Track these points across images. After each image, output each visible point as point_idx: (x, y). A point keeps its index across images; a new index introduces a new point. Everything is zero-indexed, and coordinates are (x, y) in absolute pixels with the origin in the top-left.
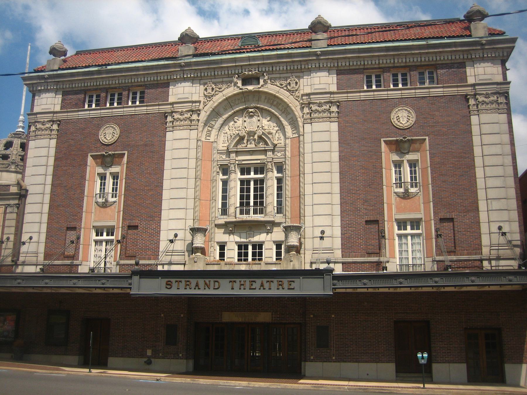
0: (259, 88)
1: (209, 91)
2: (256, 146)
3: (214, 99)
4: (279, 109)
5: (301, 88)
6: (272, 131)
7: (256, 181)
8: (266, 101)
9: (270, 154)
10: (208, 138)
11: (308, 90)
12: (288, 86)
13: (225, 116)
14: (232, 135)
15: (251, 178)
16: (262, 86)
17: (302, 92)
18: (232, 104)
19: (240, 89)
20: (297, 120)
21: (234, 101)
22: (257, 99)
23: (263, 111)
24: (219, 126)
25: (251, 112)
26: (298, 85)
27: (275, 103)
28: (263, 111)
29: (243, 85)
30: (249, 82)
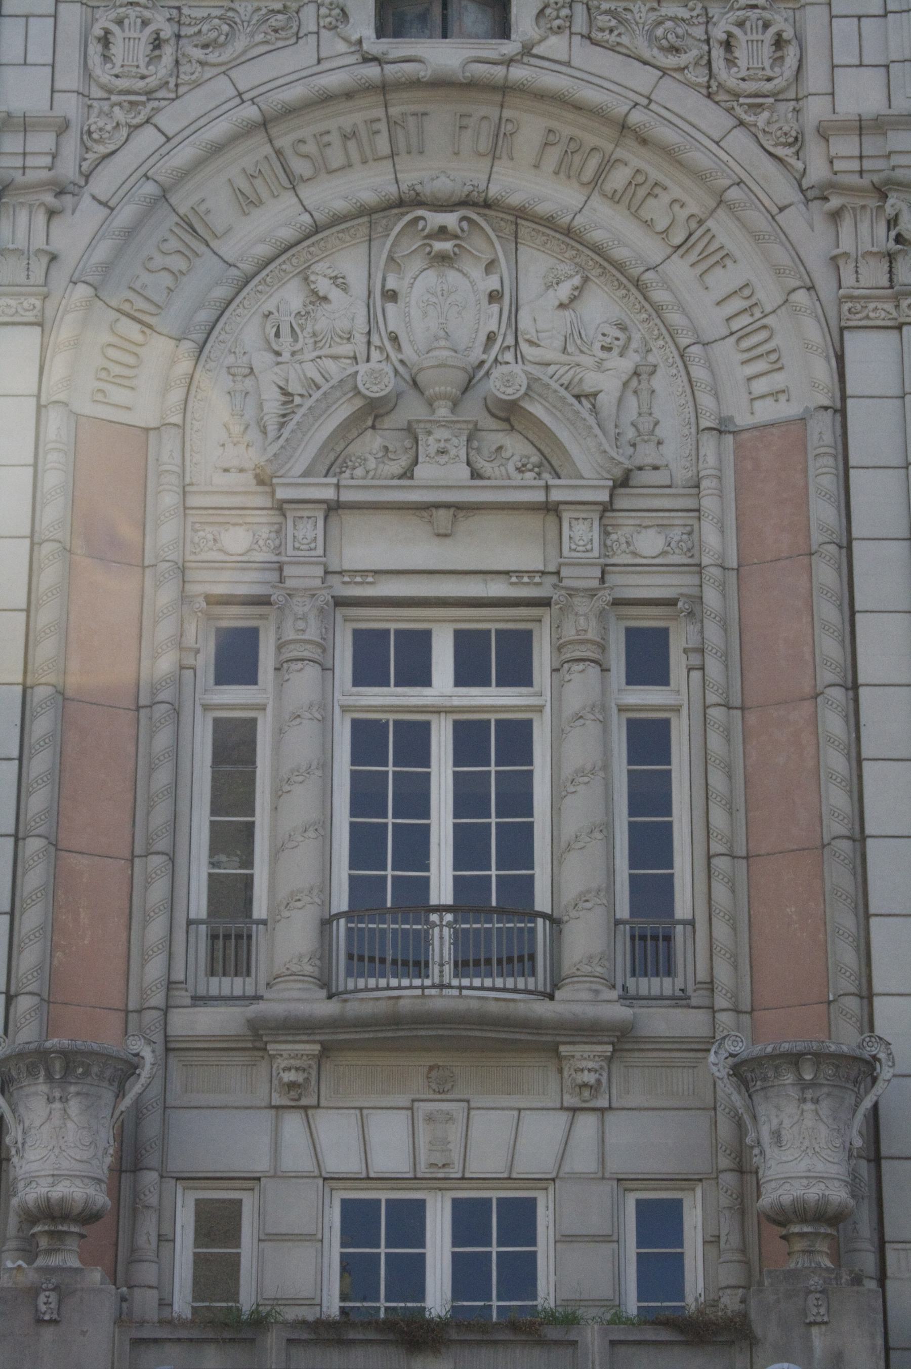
0: (509, 62)
1: (130, 48)
2: (476, 474)
3: (171, 119)
4: (648, 224)
5: (815, 78)
6: (592, 381)
7: (470, 737)
8: (553, 156)
9: (581, 533)
10: (119, 395)
11: (861, 95)
12: (719, 63)
13: (330, 195)
14: (294, 387)
15: (438, 711)
16: (527, 50)
17: (816, 110)
18: (300, 167)
19: (367, 59)
20: (8, 1160)
21: (310, 148)
22: (484, 145)
23: (525, 228)
24: (340, 206)
25: (442, 232)
26: (791, 61)
27: (618, 178)
28: (525, 228)
29: (381, 32)
30: (423, 18)
